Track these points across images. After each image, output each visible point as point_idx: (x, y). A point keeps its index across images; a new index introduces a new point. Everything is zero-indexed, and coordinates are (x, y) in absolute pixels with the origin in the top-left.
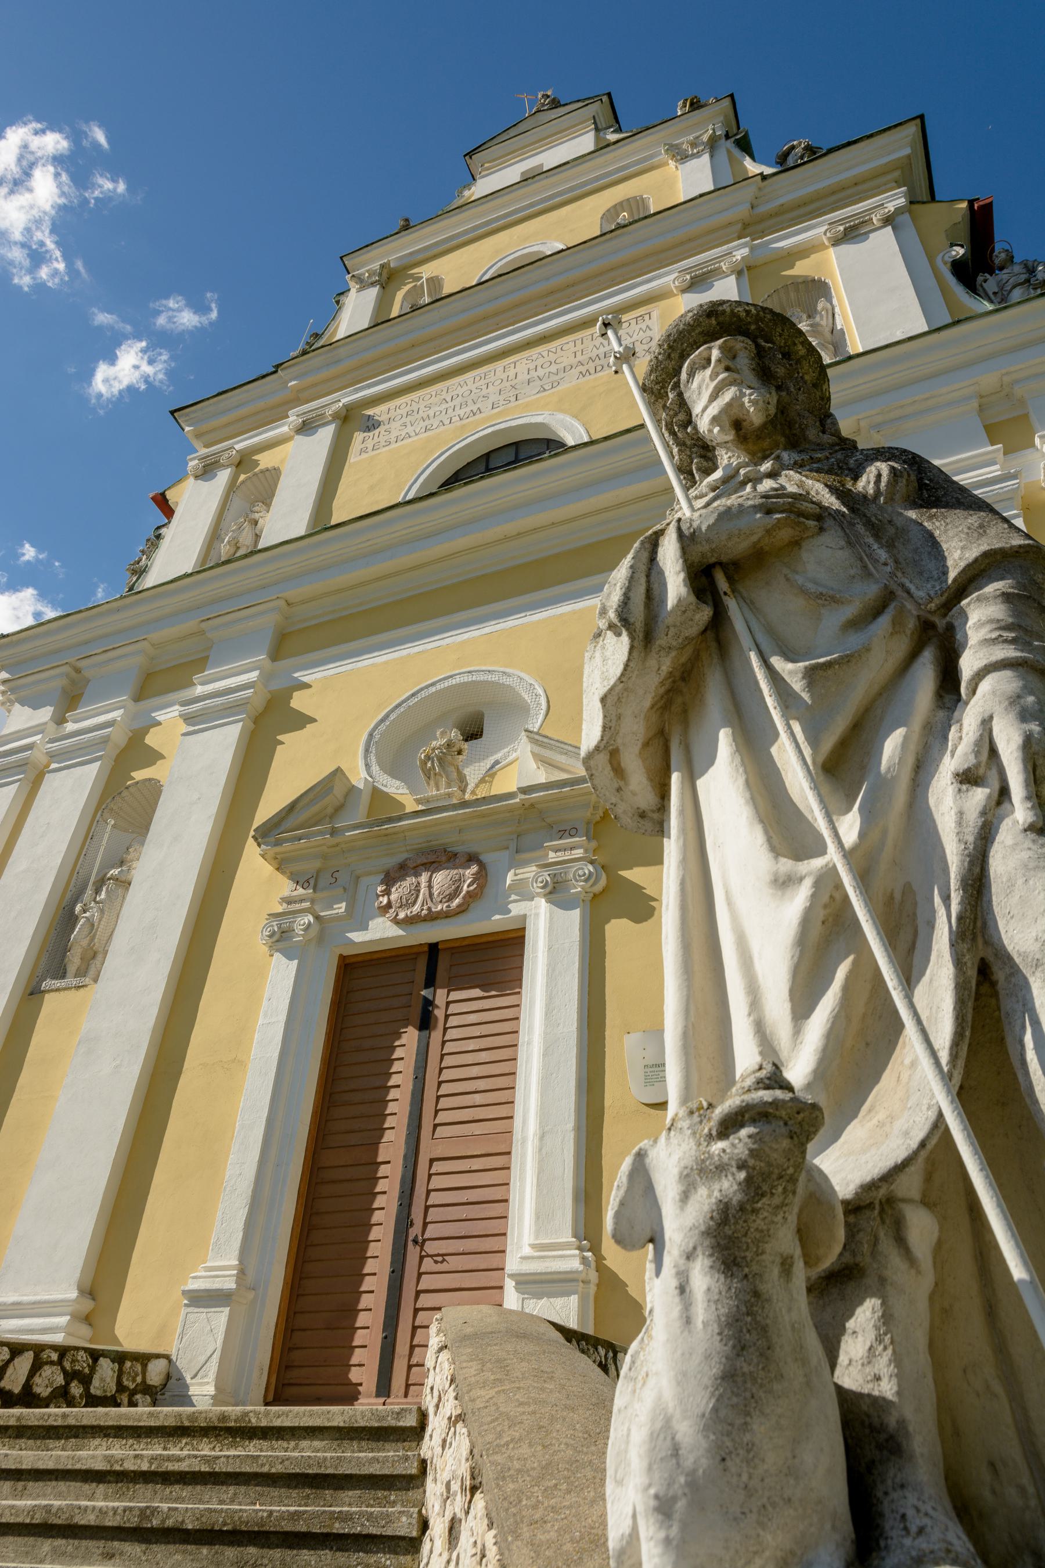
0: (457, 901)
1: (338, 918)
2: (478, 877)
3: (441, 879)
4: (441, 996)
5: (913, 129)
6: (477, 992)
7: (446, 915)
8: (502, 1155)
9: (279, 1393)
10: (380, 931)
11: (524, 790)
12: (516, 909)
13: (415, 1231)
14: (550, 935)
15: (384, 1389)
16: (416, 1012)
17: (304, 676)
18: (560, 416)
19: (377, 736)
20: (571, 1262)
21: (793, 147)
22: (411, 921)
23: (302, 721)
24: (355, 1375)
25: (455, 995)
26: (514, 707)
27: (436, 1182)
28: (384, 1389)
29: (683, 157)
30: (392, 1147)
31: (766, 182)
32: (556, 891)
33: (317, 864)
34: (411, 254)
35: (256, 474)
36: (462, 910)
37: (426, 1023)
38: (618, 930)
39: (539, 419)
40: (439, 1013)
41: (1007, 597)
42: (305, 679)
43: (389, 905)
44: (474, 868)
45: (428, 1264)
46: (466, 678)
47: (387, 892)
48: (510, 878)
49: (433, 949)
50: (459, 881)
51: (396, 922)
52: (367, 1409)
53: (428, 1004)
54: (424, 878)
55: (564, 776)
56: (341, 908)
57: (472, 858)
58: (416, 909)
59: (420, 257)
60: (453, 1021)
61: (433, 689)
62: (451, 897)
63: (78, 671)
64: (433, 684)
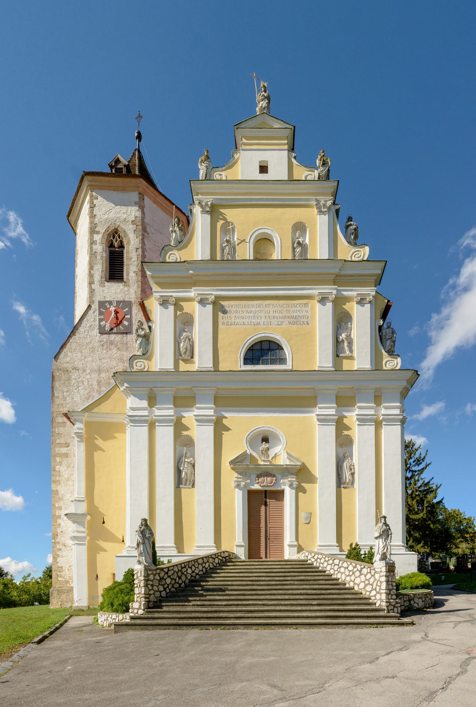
0: (272, 484)
1: (248, 483)
2: (276, 480)
3: (269, 479)
4: (268, 500)
5: (383, 264)
6: (274, 501)
7: (270, 486)
8: (282, 528)
9: (249, 558)
10: (256, 487)
11: (286, 465)
12: (283, 487)
13: (268, 538)
14: (289, 494)
15: (266, 557)
16: (264, 503)
17: (226, 414)
18: (284, 340)
19: (248, 439)
20: (296, 543)
21: (351, 225)
22: (263, 486)
23: (228, 429)
24: (261, 556)
25: (270, 501)
26: (277, 438)
27: (270, 531)
28: (266, 557)
29: (320, 212)
30: (263, 525)
31: (345, 263)
32: (291, 486)
33: (242, 471)
34: (221, 199)
35: (183, 313)
36: (273, 485)
37: (266, 505)
38: (300, 494)
39: (277, 337)
40: (268, 504)
41: (345, 305)
42: (225, 415)
43: (259, 482)
44: (275, 478)
45: (271, 542)
46: (267, 429)
47: (258, 480)
48: (281, 481)
49: (266, 491)
50: (272, 480)
51: (260, 486)
52: (264, 559)
53: (266, 502)
54: (265, 478)
55: (294, 464)
56: (249, 481)
57: (274, 476)
58: (264, 484)
59: (224, 203)
60: (270, 505)
61: (259, 429)
62: (271, 483)
63: (151, 390)
64: (259, 428)
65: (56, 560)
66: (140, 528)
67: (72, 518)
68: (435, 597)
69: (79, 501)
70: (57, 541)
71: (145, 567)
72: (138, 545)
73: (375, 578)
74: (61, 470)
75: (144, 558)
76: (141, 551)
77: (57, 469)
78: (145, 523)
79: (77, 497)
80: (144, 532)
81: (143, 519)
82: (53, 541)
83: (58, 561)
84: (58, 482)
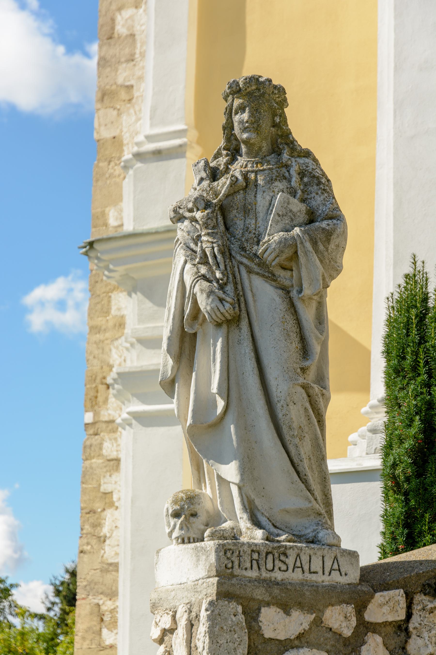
65: (97, 525)
66: (214, 175)
67: (118, 262)
68: (235, 443)
69: (158, 155)
70: (105, 415)
71: (226, 574)
72: (185, 345)
73: (255, 560)
74: (137, 28)
75: (231, 471)
76: (203, 406)
77: (121, 29)
78: (254, 125)
79: (149, 138)
80: (247, 210)
81: (235, 90)
82: (89, 417)
83: (105, 530)
84: (123, 95)
